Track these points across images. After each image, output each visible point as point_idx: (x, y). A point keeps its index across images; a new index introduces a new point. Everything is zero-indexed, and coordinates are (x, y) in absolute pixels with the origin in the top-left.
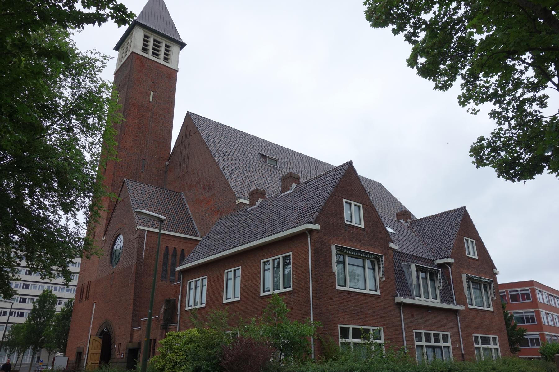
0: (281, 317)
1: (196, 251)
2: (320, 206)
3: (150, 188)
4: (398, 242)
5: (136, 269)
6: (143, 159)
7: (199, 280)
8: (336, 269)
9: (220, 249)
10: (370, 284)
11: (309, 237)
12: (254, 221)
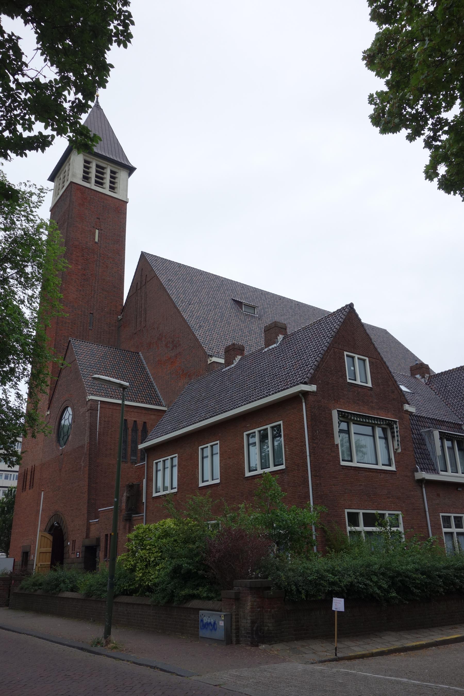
0: (276, 502)
1: (162, 424)
2: (316, 362)
3: (101, 349)
4: (415, 403)
5: (90, 449)
6: (91, 313)
7: (168, 459)
8: (338, 439)
9: (192, 421)
10: (382, 456)
11: (303, 401)
12: (233, 383)
